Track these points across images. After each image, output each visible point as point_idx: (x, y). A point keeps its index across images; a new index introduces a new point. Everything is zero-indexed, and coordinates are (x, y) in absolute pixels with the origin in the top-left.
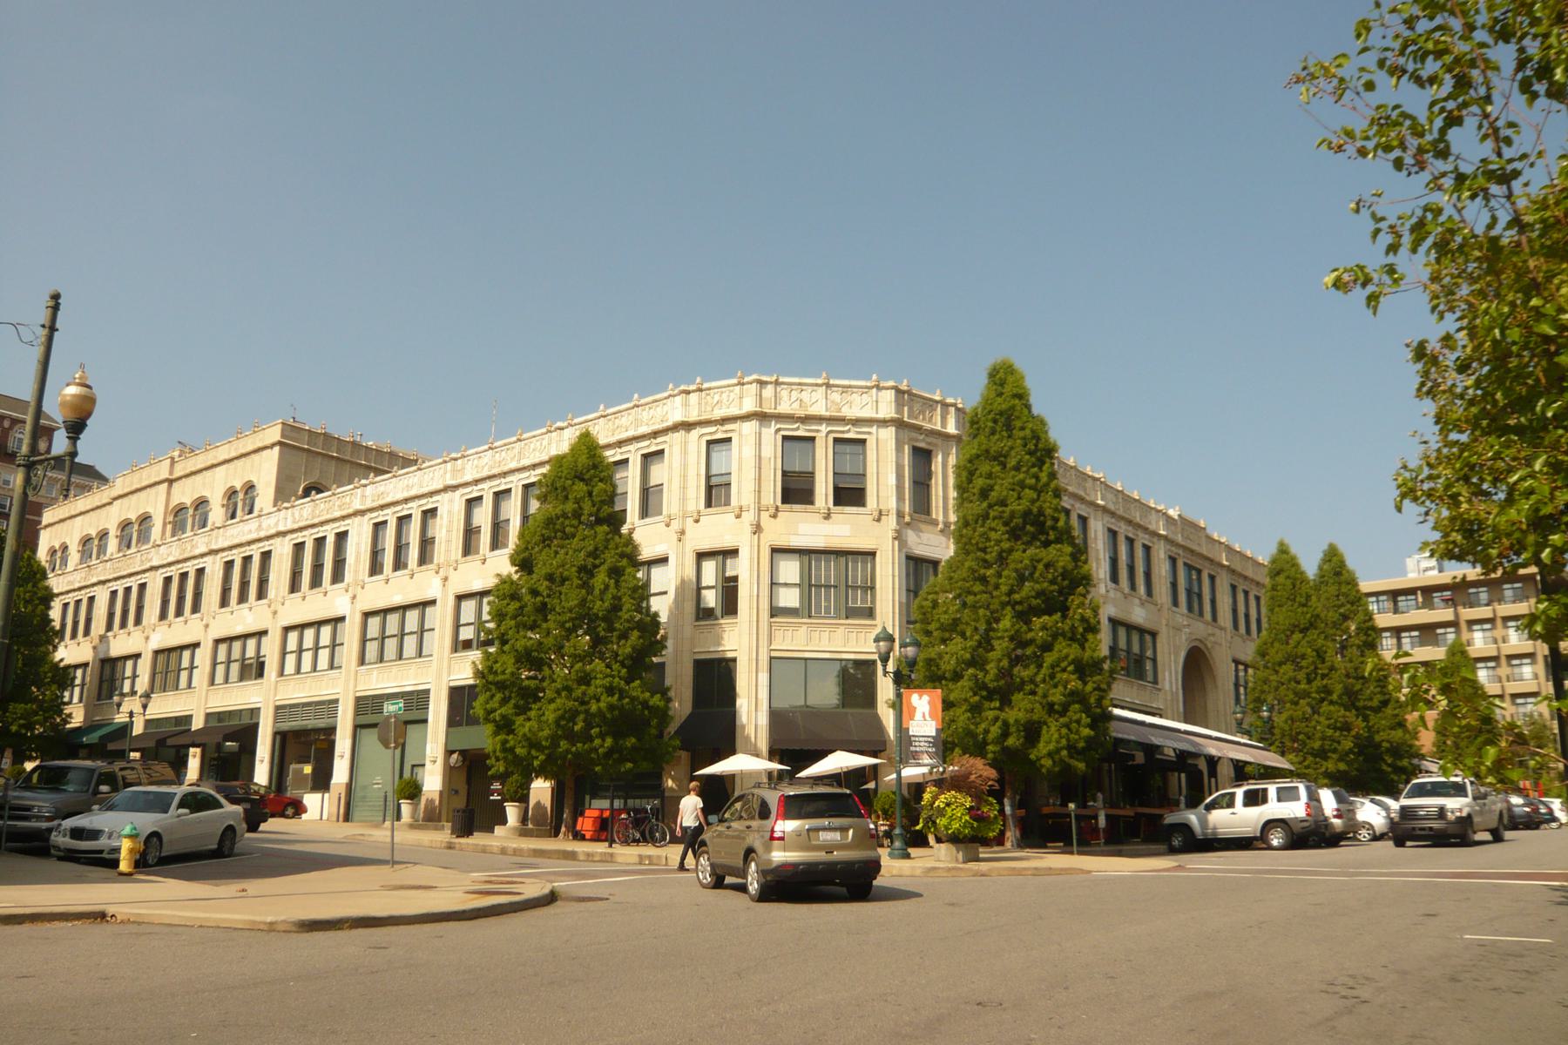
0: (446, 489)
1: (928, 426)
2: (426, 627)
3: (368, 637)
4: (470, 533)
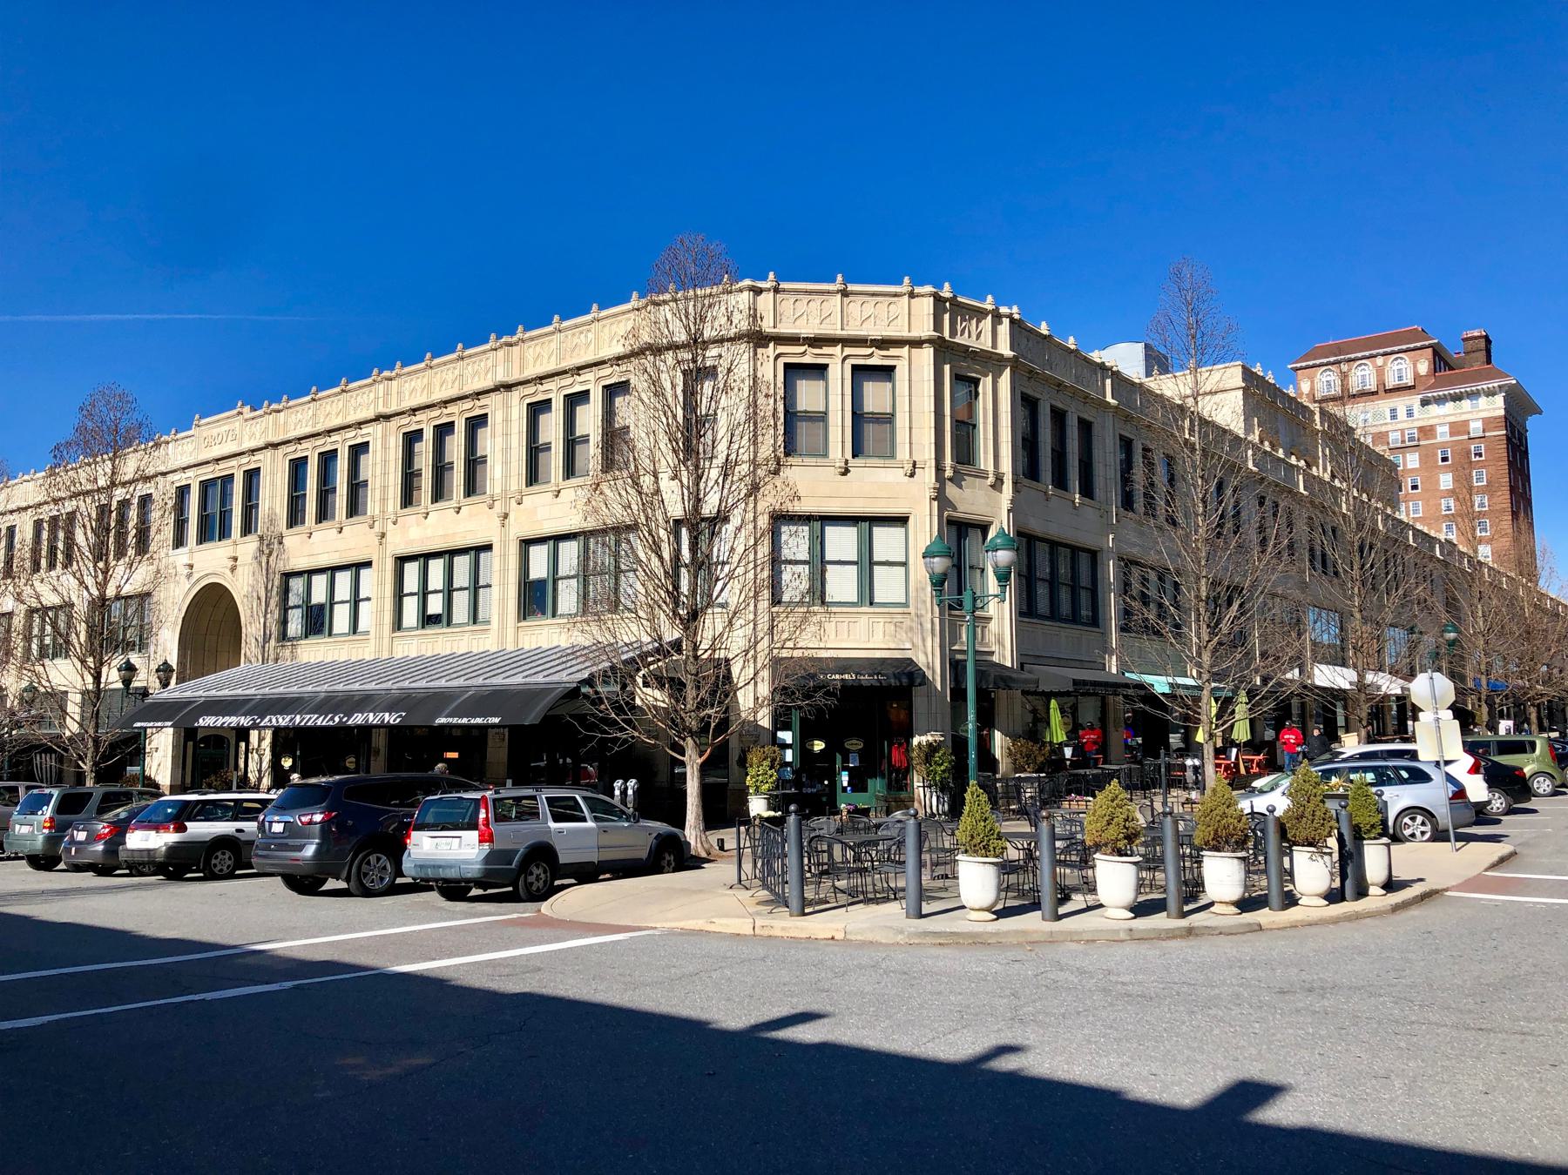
1: (972, 343)
2: (481, 583)
4: (535, 451)
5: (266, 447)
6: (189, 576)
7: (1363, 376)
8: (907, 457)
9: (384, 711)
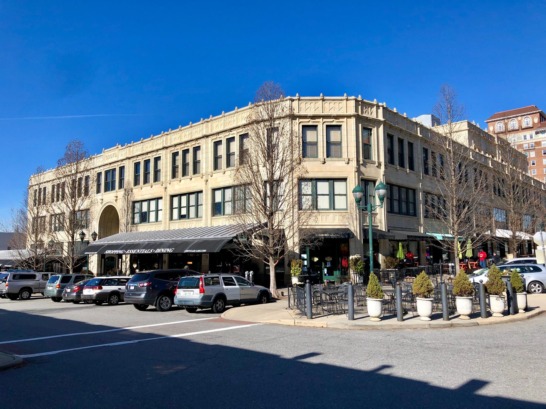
4: (216, 158)
5: (126, 159)
6: (102, 203)
8: (346, 157)
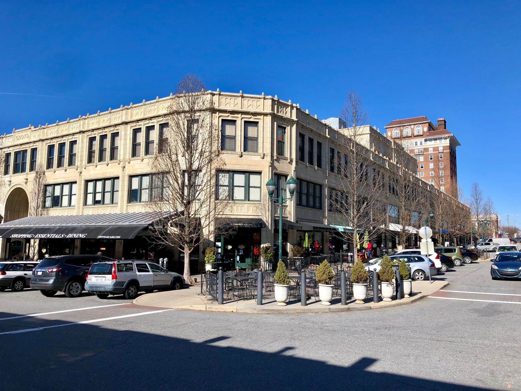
0: (80, 132)
3: (143, 187)
4: (135, 146)
7: (418, 130)
9: (28, 234)
